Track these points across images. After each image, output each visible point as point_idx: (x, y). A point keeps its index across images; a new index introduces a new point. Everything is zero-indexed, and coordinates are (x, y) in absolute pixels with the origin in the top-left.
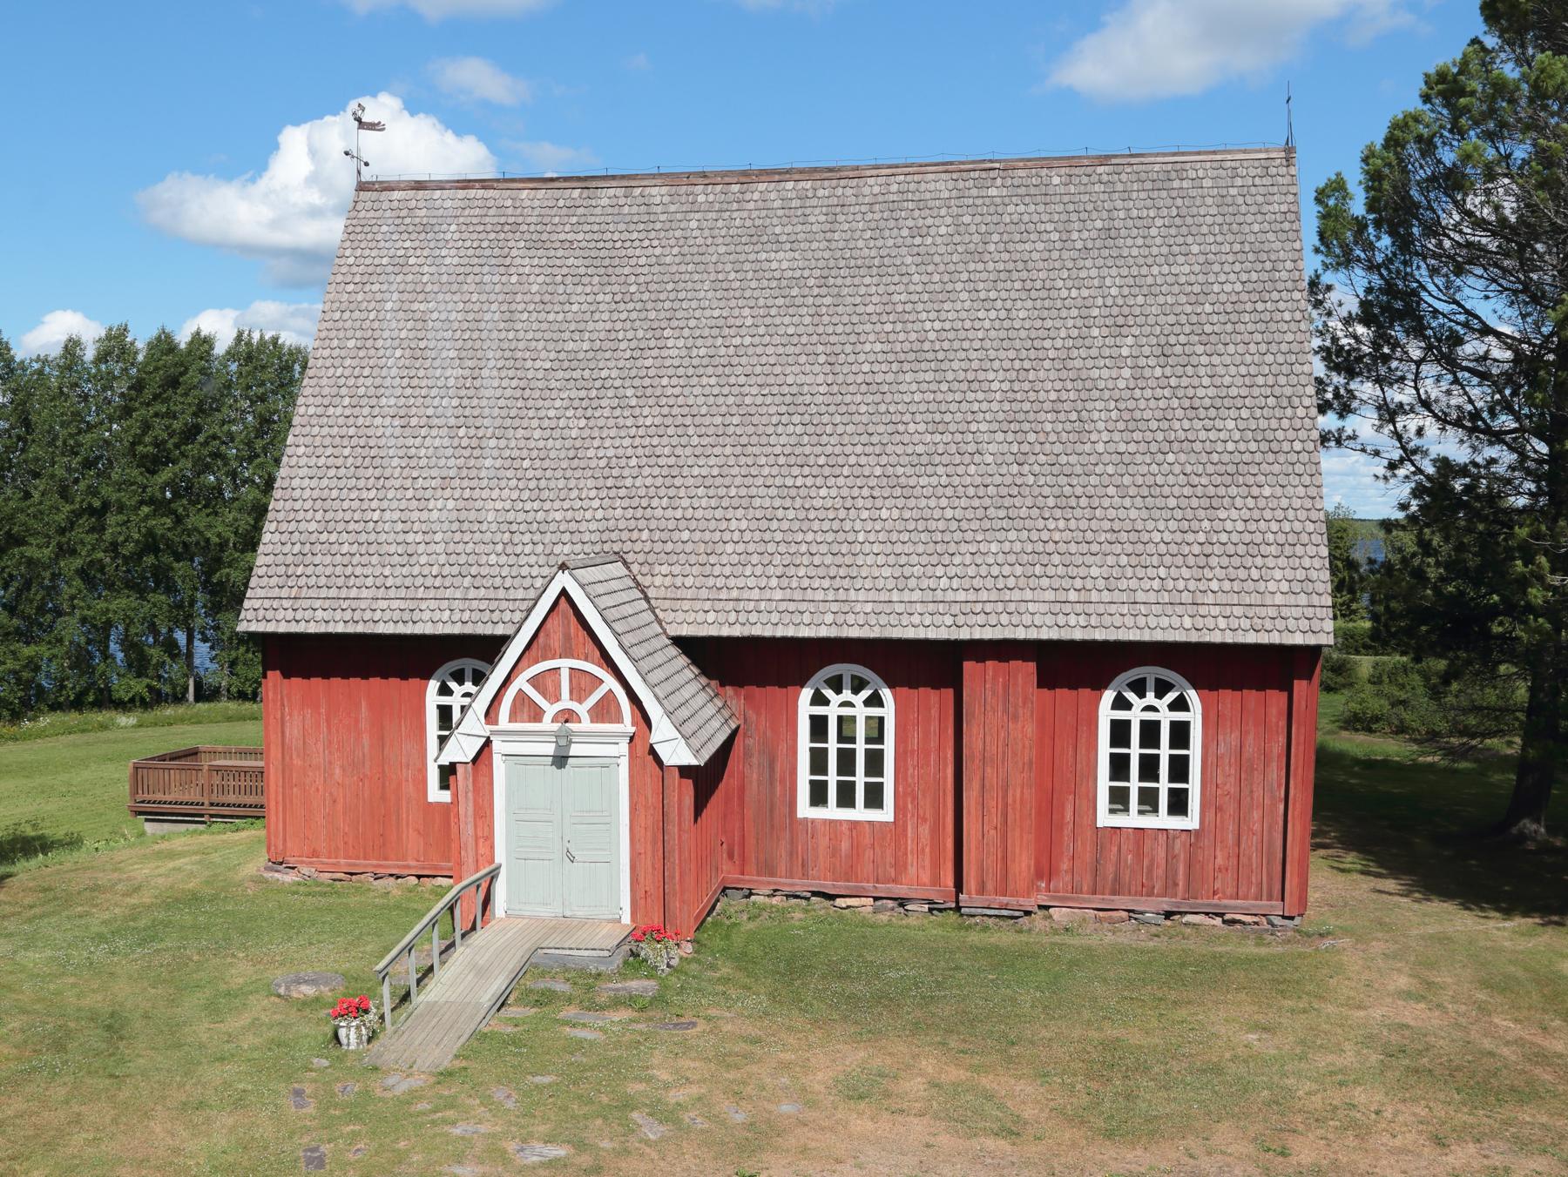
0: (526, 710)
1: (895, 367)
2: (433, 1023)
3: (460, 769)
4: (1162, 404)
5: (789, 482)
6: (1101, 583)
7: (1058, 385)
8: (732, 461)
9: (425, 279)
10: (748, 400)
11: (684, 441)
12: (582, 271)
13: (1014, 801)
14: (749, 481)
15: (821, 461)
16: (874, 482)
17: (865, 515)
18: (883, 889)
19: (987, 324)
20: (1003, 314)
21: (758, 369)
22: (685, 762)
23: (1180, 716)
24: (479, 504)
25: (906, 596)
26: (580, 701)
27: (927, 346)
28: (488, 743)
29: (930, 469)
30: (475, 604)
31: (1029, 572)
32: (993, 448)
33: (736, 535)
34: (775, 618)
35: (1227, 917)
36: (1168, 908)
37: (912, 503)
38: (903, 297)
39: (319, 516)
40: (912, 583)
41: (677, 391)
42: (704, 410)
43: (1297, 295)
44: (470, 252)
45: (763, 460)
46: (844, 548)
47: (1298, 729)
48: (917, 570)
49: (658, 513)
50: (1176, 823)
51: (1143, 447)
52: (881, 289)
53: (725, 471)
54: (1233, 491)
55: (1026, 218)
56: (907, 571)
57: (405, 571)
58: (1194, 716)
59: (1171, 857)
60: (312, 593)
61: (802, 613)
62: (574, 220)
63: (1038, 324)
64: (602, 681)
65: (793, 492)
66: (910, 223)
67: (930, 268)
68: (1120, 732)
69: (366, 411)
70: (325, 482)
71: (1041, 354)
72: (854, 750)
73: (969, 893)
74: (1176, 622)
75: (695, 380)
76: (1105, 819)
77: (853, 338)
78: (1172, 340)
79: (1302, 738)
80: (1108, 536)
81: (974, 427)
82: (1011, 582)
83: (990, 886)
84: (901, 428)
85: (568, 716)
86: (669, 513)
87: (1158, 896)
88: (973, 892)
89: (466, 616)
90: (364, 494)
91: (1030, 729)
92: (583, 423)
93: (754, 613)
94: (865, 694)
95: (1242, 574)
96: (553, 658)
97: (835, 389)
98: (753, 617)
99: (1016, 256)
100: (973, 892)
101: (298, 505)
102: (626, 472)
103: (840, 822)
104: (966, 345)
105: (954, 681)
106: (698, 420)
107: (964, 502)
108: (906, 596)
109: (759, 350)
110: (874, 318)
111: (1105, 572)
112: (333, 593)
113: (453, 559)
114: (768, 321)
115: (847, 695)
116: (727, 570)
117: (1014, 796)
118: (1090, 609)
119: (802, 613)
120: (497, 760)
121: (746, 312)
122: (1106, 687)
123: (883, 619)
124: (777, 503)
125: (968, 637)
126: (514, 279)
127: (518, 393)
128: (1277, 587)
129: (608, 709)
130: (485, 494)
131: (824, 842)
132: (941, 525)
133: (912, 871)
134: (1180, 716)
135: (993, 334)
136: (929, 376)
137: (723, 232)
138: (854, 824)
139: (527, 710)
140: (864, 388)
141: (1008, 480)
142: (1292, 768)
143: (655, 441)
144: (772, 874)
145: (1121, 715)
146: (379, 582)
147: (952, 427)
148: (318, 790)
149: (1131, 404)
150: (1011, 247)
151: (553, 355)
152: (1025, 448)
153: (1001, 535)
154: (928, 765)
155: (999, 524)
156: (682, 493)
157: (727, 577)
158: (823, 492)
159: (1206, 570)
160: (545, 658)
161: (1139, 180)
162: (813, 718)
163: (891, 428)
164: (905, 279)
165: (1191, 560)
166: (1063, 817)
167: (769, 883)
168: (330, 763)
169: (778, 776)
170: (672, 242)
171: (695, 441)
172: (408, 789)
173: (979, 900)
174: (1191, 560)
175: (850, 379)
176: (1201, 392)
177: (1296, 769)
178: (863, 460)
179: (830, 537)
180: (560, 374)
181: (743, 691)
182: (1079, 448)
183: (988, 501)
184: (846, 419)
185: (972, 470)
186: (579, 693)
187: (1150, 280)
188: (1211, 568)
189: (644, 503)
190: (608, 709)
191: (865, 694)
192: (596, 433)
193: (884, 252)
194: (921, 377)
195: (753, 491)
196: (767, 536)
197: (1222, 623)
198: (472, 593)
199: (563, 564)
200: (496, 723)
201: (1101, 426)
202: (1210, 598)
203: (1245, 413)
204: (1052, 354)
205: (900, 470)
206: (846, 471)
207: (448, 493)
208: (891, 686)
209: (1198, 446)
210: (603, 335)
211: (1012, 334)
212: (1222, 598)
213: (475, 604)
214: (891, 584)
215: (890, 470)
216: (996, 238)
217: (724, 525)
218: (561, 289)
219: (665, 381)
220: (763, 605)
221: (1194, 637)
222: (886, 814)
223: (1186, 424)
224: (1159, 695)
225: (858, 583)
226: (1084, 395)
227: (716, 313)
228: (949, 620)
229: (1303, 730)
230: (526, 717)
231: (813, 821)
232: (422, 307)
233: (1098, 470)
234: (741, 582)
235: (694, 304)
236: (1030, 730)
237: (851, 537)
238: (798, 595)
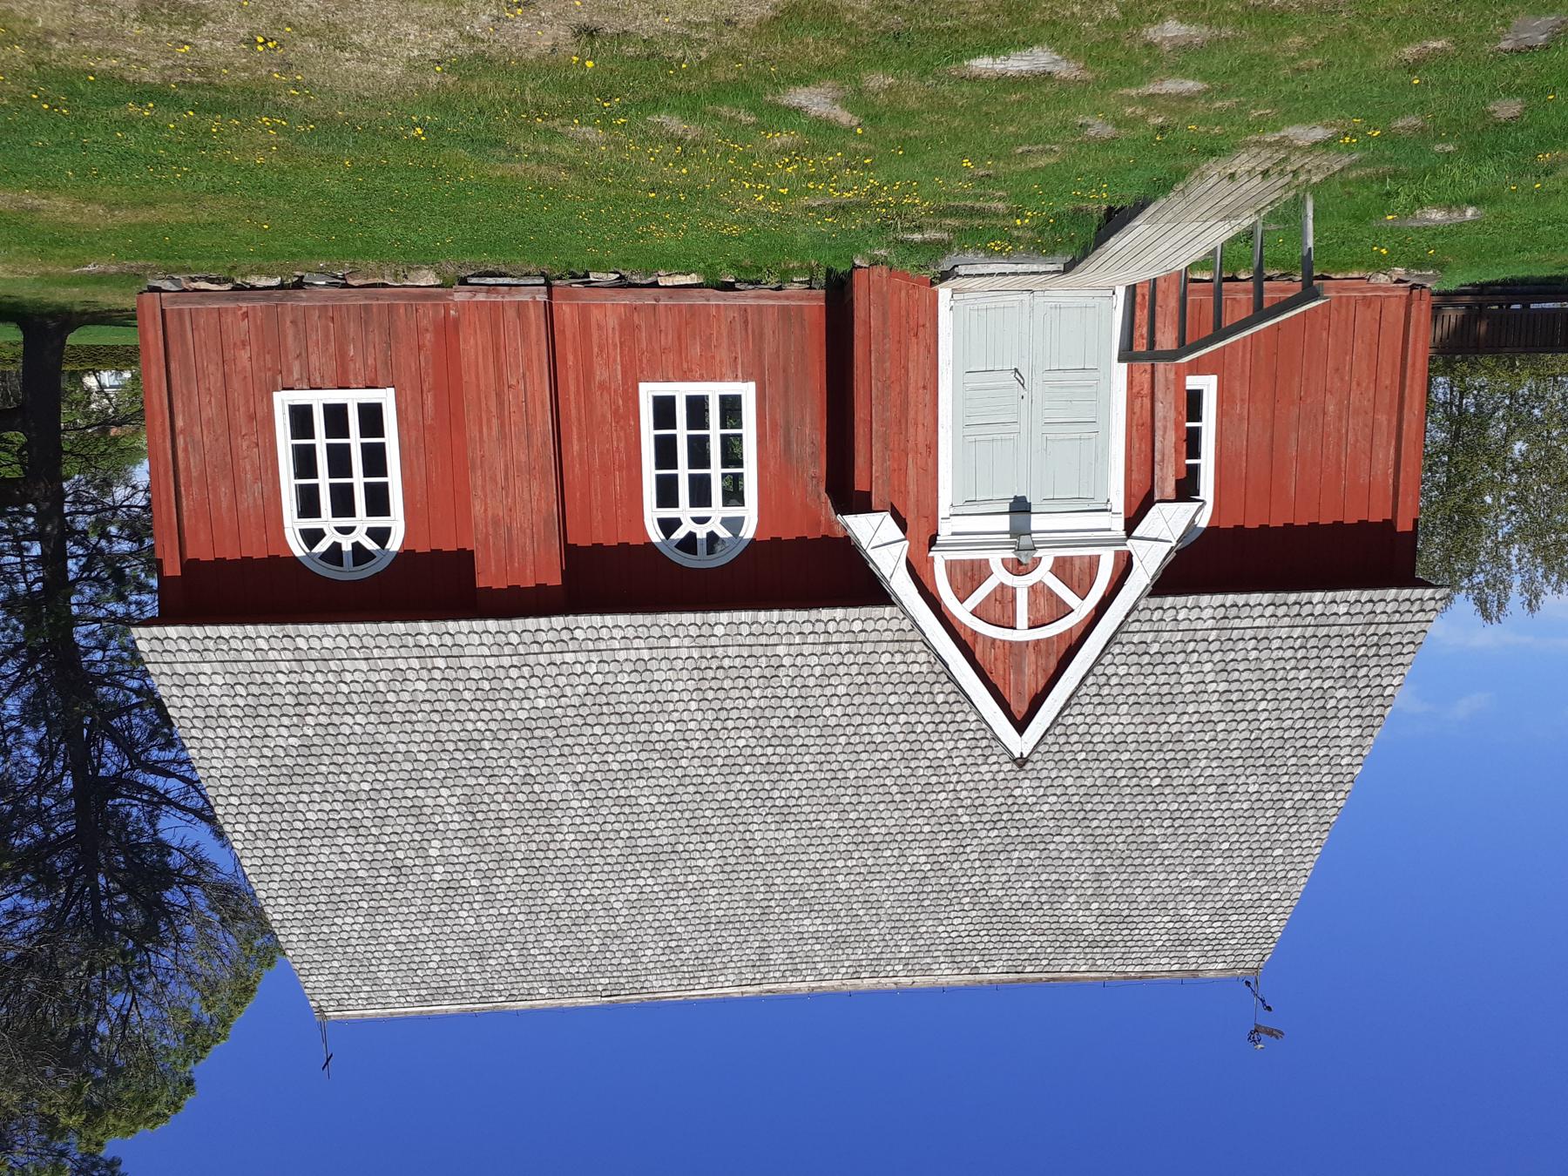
0: (1076, 572)
1: (680, 848)
2: (1230, 199)
3: (1170, 489)
4: (389, 830)
5: (780, 750)
6: (411, 675)
7: (503, 840)
8: (847, 766)
9: (1192, 904)
10: (835, 816)
11: (901, 781)
12: (1020, 913)
13: (489, 421)
14: (825, 749)
15: (747, 769)
16: (689, 753)
17: (692, 725)
18: (647, 298)
19: (589, 884)
20: (574, 893)
21: (826, 841)
22: (862, 517)
23: (311, 523)
24: (1137, 720)
25: (633, 655)
26: (1002, 586)
27: (650, 866)
28: (1131, 524)
29: (627, 766)
30: (1146, 627)
31: (496, 684)
32: (563, 787)
33: (835, 701)
34: (782, 629)
35: (228, 286)
36: (301, 293)
37: (641, 738)
38: (680, 902)
39: (1332, 703)
40: (628, 667)
41: (912, 822)
42: (881, 807)
43: (278, 916)
44: (1141, 926)
45: (812, 767)
46: (710, 695)
47: (170, 519)
48: (624, 678)
49: (926, 718)
50: (664, 389)
51: (398, 794)
52: (704, 907)
53: (853, 757)
54: (288, 761)
55: (567, 963)
56: (635, 677)
57: (1232, 655)
58: (293, 524)
59: (303, 356)
60: (1350, 630)
61: (751, 634)
62: (1030, 951)
63: (536, 887)
64: (974, 613)
65: (775, 741)
66: (682, 956)
67: (656, 924)
68: (378, 502)
69: (1266, 797)
70: (1320, 734)
71: (527, 863)
72: (690, 467)
73: (535, 302)
74: (315, 643)
75: (894, 830)
76: (386, 398)
77: (728, 869)
78: (393, 880)
79: (164, 508)
80: (414, 718)
81: (586, 803)
82: (514, 673)
83: (511, 313)
84: (665, 799)
85: (1018, 568)
86: (913, 719)
87: (314, 307)
88: (531, 305)
89: (1157, 615)
90: (1275, 725)
91: (477, 508)
92: (1017, 792)
93: (807, 632)
94: (679, 534)
95: (254, 689)
96: (1038, 642)
97: (741, 828)
98: (807, 628)
99: (572, 936)
100: (531, 305)
101: (1357, 711)
102: (965, 752)
103: (702, 379)
104: (607, 868)
105: (573, 555)
106: (888, 798)
107: (584, 740)
108: (633, 655)
109: (826, 857)
110: (708, 884)
111: (409, 686)
112: (1322, 631)
113: (1171, 669)
114: (820, 880)
115: (701, 532)
116: (842, 670)
117: (490, 428)
118: (416, 652)
119: (751, 634)
120: (1118, 503)
121: (843, 886)
122: (398, 554)
123: (656, 632)
124: (792, 732)
125: (553, 619)
126: (1095, 906)
127: (1090, 816)
128: (214, 682)
129: (969, 576)
130: (1131, 728)
131: (723, 354)
132: (605, 720)
133: (612, 322)
134: (311, 523)
135: (582, 878)
136: (642, 842)
137: (874, 944)
138: (685, 377)
139: (1076, 574)
140: (710, 829)
141: (538, 761)
142: (171, 473)
143: (934, 780)
144: (784, 309)
145: (379, 522)
146: (1265, 643)
147: (608, 802)
148: (1358, 384)
149: (421, 828)
150: (578, 943)
151: (1052, 847)
152: (526, 789)
153: (534, 714)
154: (601, 454)
155: (540, 723)
156: (900, 737)
157: (842, 663)
158: (741, 743)
159: (296, 691)
160: (1048, 640)
161: (462, 993)
162: (741, 502)
163: (676, 799)
164: (680, 915)
165: (315, 699)
166: (435, 397)
167: (787, 298)
168: (1340, 419)
169: (781, 432)
170: (925, 936)
171: (889, 781)
172: (1240, 389)
173: (523, 296)
174: (315, 699)
175: (726, 837)
176: (351, 840)
177: (166, 472)
178: (702, 771)
179: (728, 704)
180: (1043, 831)
181: (823, 531)
182: (467, 791)
183: (558, 742)
184: (726, 805)
185: (580, 768)
186: (1004, 597)
187: (430, 923)
188: (290, 693)
189: (943, 727)
190: (969, 576)
191: (679, 534)
192: (1002, 785)
193: (707, 934)
194: (651, 841)
195: (820, 741)
196: (799, 702)
197: (262, 643)
198: (1150, 637)
199: (1021, 766)
200: (1117, 554)
201: (448, 809)
202: (283, 666)
203: (299, 825)
204: (516, 864)
205: (660, 764)
206: (720, 761)
207: (1175, 729)
208: (650, 546)
209: (339, 796)
210: (997, 863)
211: (562, 878)
212: (271, 667)
213: (1146, 627)
214: (653, 665)
215: (671, 763)
216: (594, 949)
217: (850, 710)
218: (1044, 899)
219: (926, 829)
220: (797, 640)
221: (290, 629)
222: (648, 391)
223: (357, 814)
224: (336, 546)
225: (690, 664)
226: (473, 833)
227: (875, 884)
228: (579, 634)
229: (164, 517)
230: (1077, 563)
231: (736, 379)
232: (1196, 883)
233: (441, 774)
234: (825, 660)
235: (899, 890)
236: (477, 508)
237: (705, 705)
238: (758, 651)
